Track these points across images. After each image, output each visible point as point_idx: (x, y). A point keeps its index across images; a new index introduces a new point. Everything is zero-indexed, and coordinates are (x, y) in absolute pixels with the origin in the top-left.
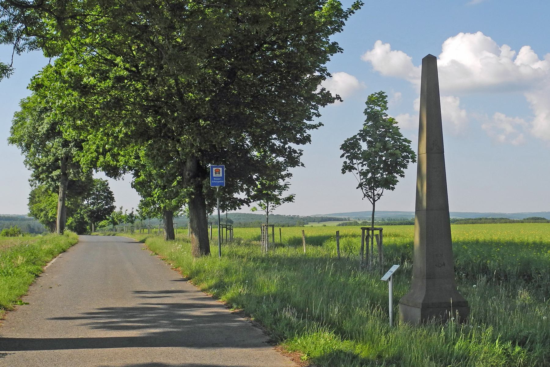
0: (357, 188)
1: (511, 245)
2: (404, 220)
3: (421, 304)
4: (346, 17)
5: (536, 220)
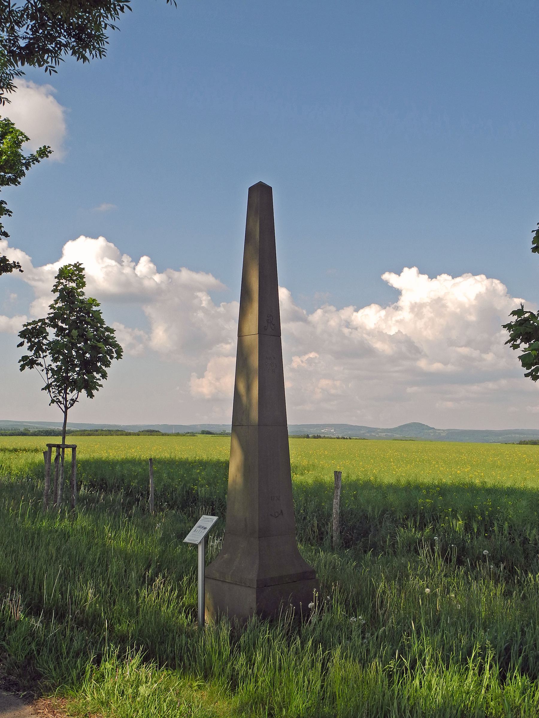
0: (43, 389)
1: (171, 463)
2: (15, 430)
3: (256, 581)
4: (27, 165)
5: (151, 432)
